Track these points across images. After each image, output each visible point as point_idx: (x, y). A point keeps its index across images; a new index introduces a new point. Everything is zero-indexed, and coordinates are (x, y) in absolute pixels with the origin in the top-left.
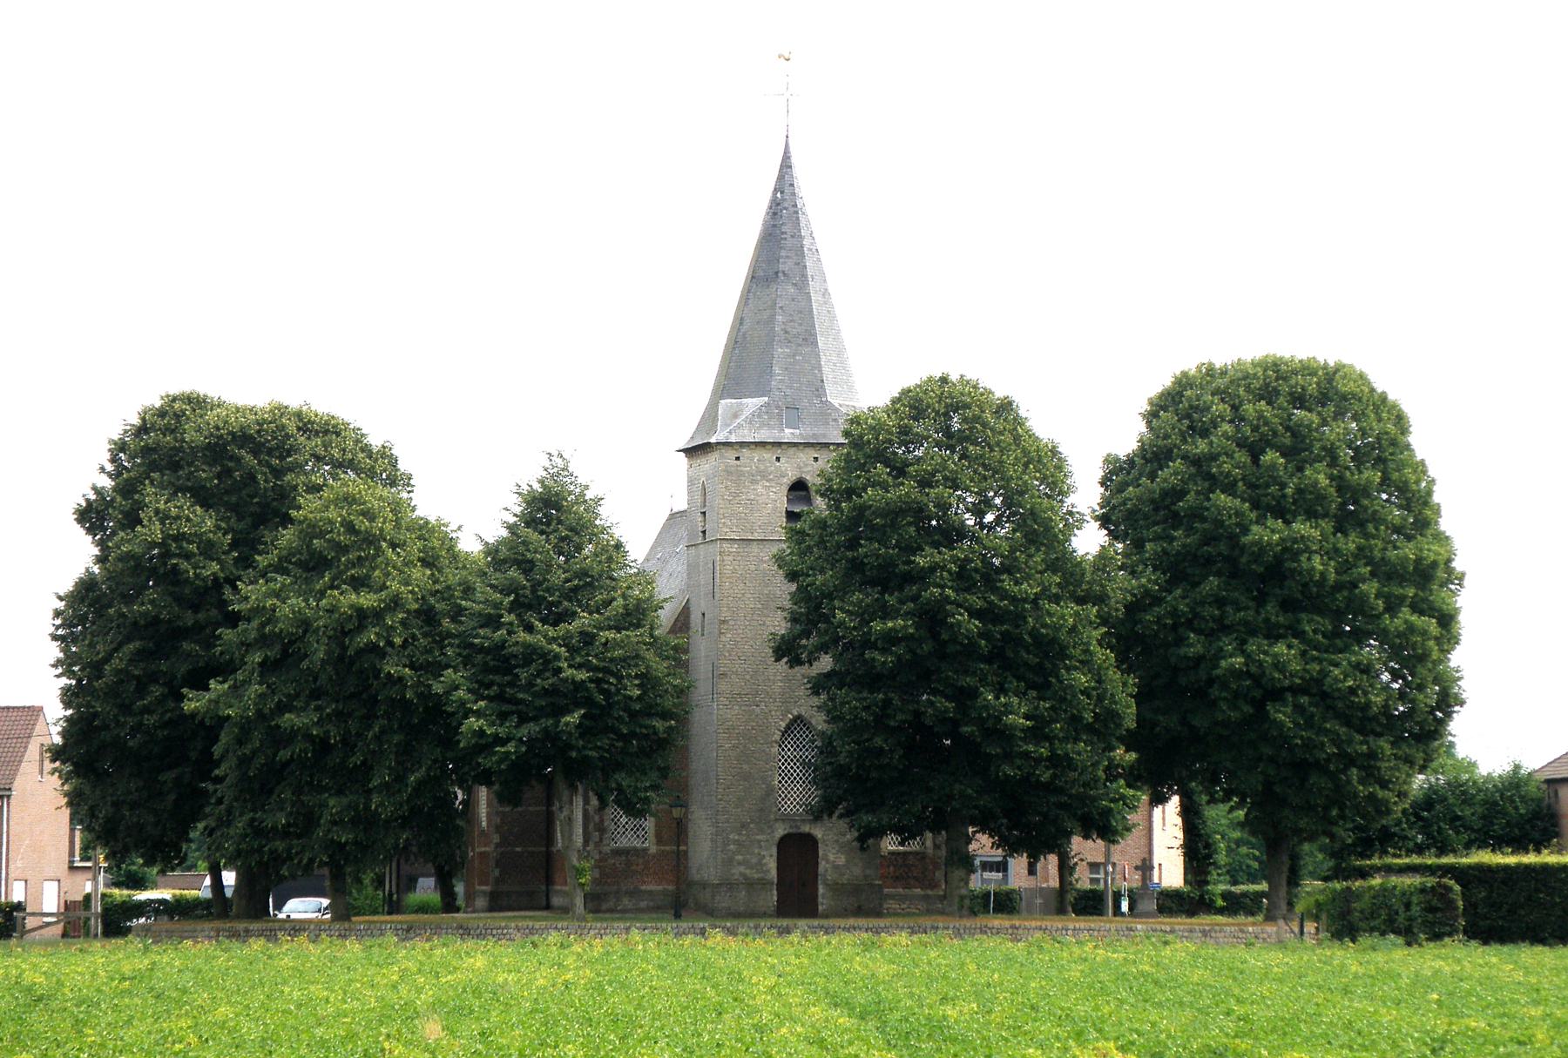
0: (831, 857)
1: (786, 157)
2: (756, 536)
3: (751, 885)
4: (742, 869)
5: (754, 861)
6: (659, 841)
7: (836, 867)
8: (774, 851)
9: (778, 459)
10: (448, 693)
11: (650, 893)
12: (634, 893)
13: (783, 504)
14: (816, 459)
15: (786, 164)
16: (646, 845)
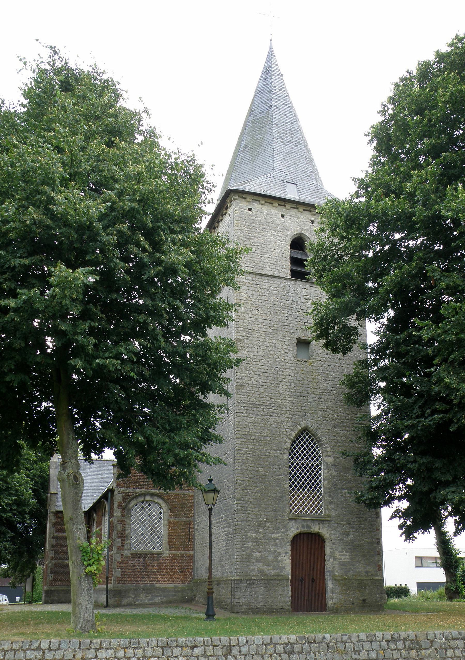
0: (337, 555)
1: (271, 51)
2: (266, 272)
3: (270, 581)
4: (260, 565)
5: (271, 557)
6: (172, 545)
8: (289, 548)
9: (283, 216)
10: (25, 454)
11: (164, 590)
12: (149, 591)
13: (287, 251)
14: (312, 222)
15: (271, 51)
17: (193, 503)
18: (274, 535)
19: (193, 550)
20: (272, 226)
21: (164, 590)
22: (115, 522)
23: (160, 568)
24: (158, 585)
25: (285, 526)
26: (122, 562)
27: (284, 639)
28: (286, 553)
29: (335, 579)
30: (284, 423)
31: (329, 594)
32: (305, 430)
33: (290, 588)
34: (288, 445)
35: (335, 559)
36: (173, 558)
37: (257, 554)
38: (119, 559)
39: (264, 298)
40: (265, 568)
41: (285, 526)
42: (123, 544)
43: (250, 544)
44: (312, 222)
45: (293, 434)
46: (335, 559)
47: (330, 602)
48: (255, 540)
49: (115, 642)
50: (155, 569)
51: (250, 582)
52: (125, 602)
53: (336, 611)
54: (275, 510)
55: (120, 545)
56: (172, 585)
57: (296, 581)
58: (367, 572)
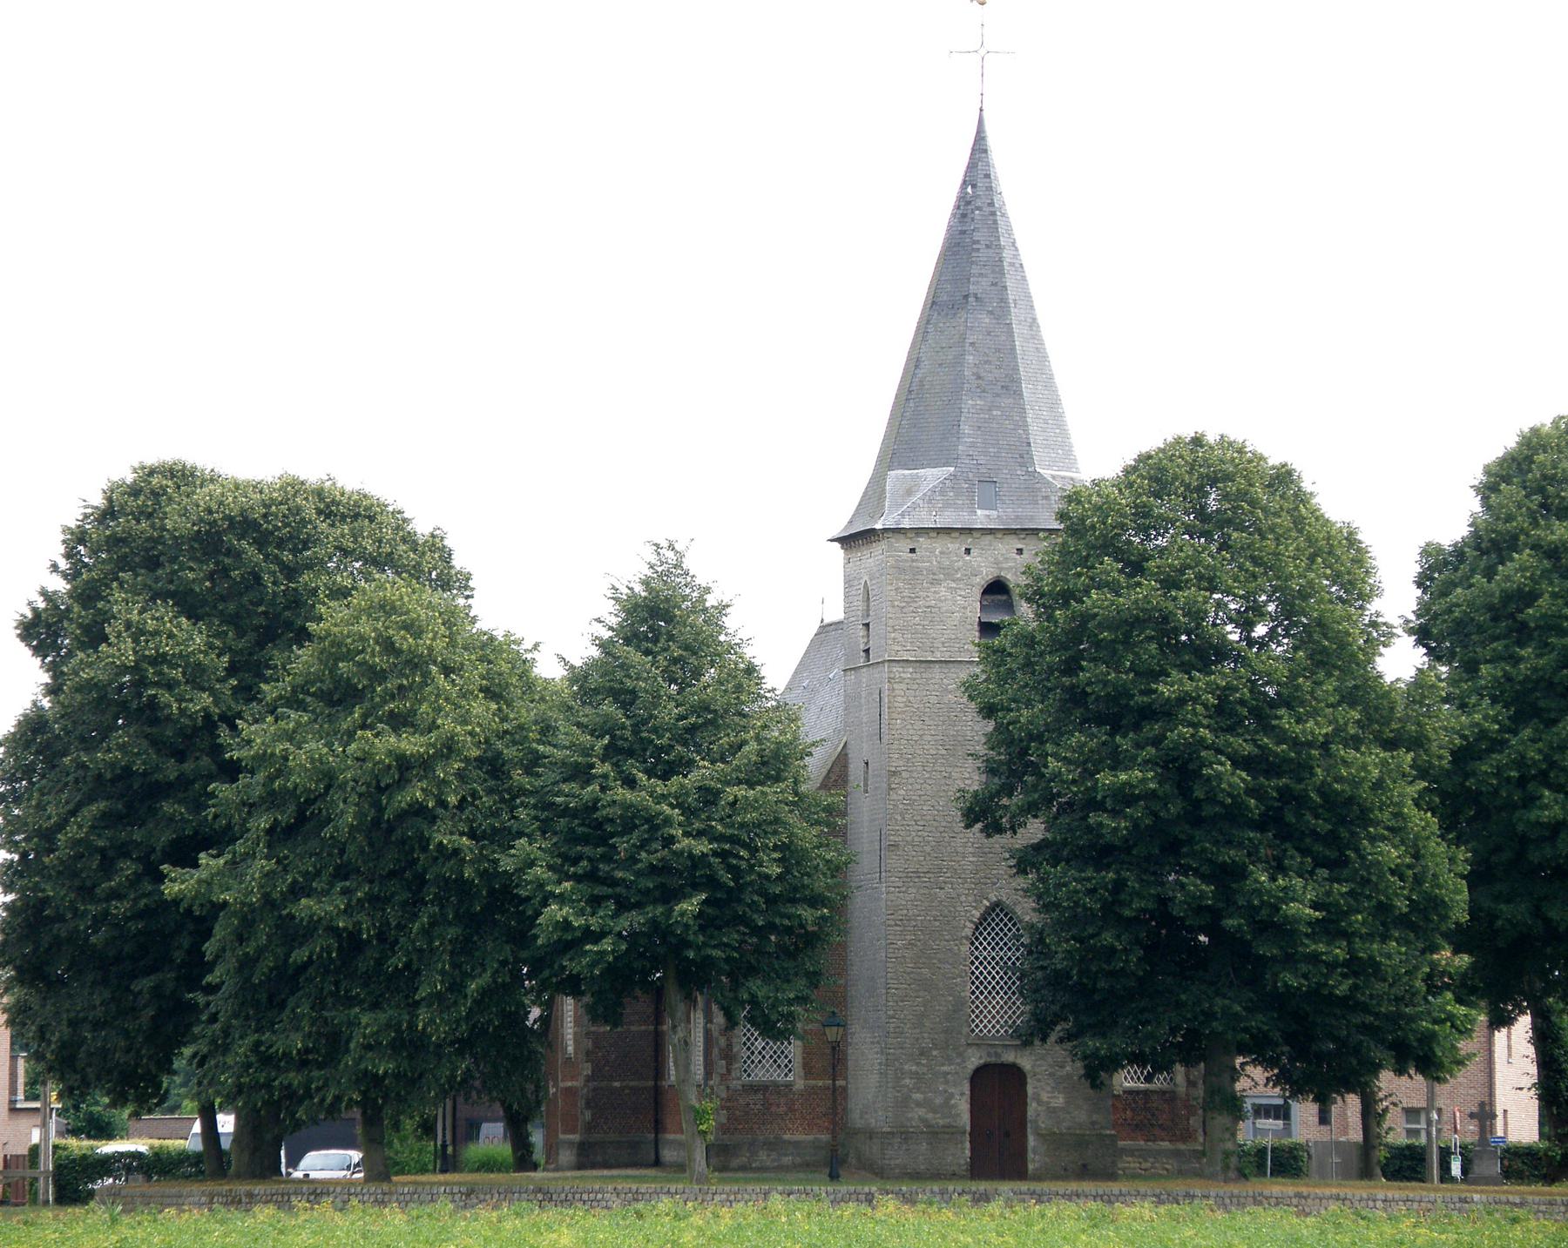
0: (1044, 1097)
3: (938, 1135)
4: (921, 1112)
5: (938, 1101)
7: (1052, 1111)
9: (968, 551)
11: (796, 1144)
12: (774, 1145)
14: (1020, 551)
15: (980, 147)
16: (791, 1078)
17: (845, 998)
18: (945, 1068)
19: (845, 1079)
20: (949, 573)
21: (796, 1144)
22: (715, 1034)
23: (791, 1110)
24: (787, 1137)
25: (960, 1055)
26: (729, 1100)
27: (866, 1189)
28: (962, 1094)
29: (1038, 1135)
30: (963, 898)
31: (1030, 1155)
32: (997, 906)
33: (968, 1145)
34: (968, 932)
35: (1039, 1102)
36: (810, 1092)
37: (918, 1096)
38: (724, 1095)
39: (933, 700)
40: (930, 1116)
41: (960, 1055)
42: (729, 1071)
43: (907, 1081)
44: (1020, 551)
45: (977, 914)
46: (1039, 1102)
47: (1031, 1167)
48: (916, 1075)
49: (727, 1188)
50: (782, 1109)
51: (905, 1135)
52: (735, 1163)
53: (1038, 1178)
54: (946, 1032)
55: (724, 1071)
56: (811, 1137)
57: (979, 1134)
58: (1093, 1123)
